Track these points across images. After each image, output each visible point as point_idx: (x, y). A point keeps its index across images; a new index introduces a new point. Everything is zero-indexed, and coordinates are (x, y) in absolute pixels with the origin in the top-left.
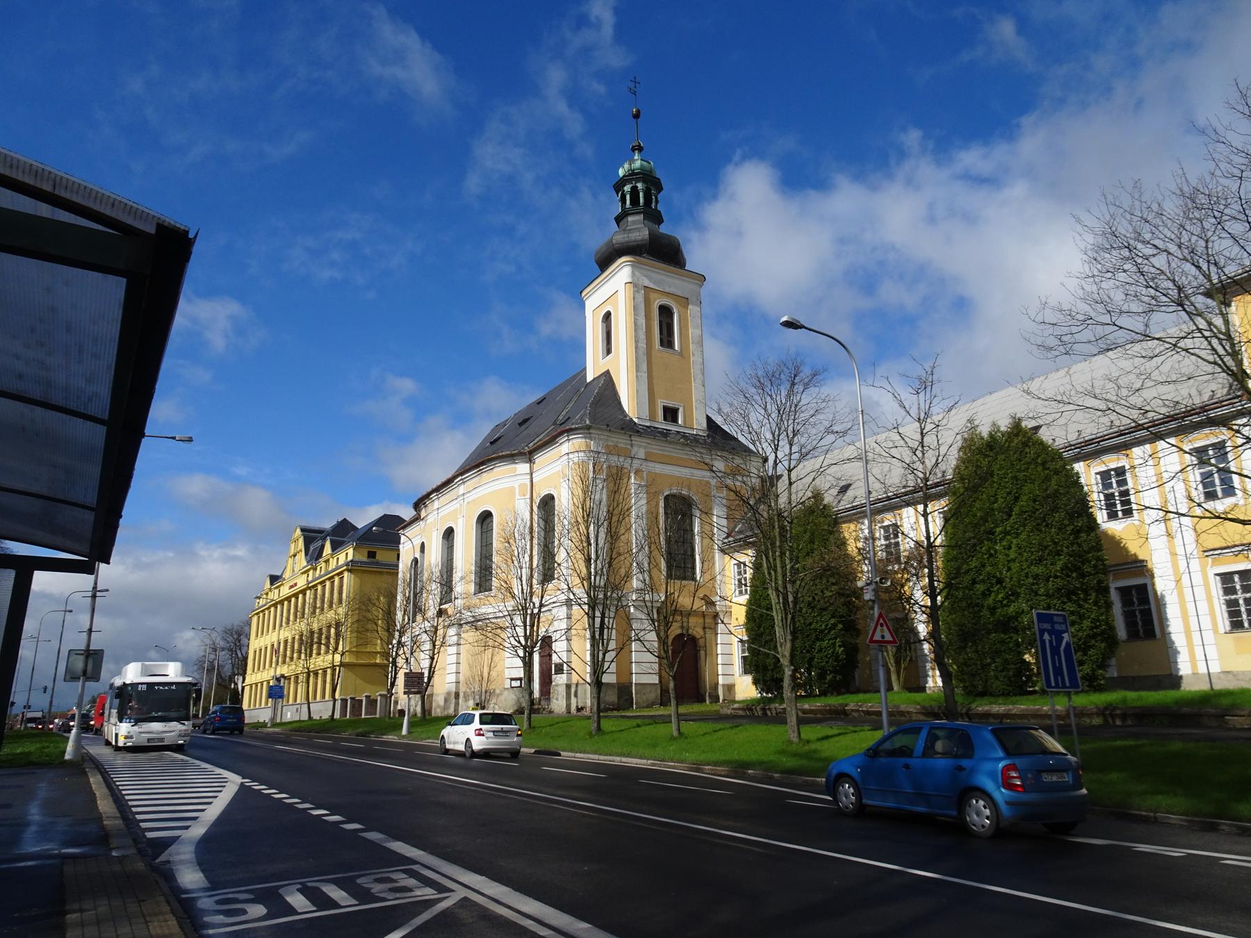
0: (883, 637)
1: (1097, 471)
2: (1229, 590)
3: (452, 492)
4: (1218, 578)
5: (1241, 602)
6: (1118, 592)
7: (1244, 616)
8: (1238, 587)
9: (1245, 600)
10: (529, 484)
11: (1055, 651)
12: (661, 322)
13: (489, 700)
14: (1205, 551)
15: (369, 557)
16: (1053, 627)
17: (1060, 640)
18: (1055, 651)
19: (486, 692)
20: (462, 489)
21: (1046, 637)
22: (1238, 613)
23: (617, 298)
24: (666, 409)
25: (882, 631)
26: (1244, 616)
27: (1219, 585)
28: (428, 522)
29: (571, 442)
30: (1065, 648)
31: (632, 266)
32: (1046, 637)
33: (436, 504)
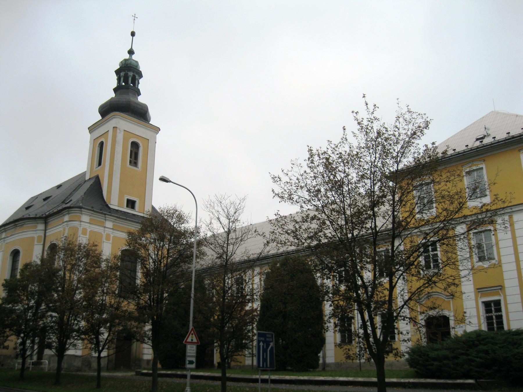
0: (192, 340)
5: (494, 317)
6: (483, 304)
7: (495, 325)
8: (493, 309)
10: (43, 236)
11: (265, 351)
12: (131, 152)
14: (478, 289)
16: (265, 339)
17: (268, 346)
18: (265, 351)
21: (261, 344)
22: (492, 324)
23: (108, 135)
24: (128, 201)
25: (192, 337)
26: (495, 325)
30: (270, 349)
32: (261, 344)
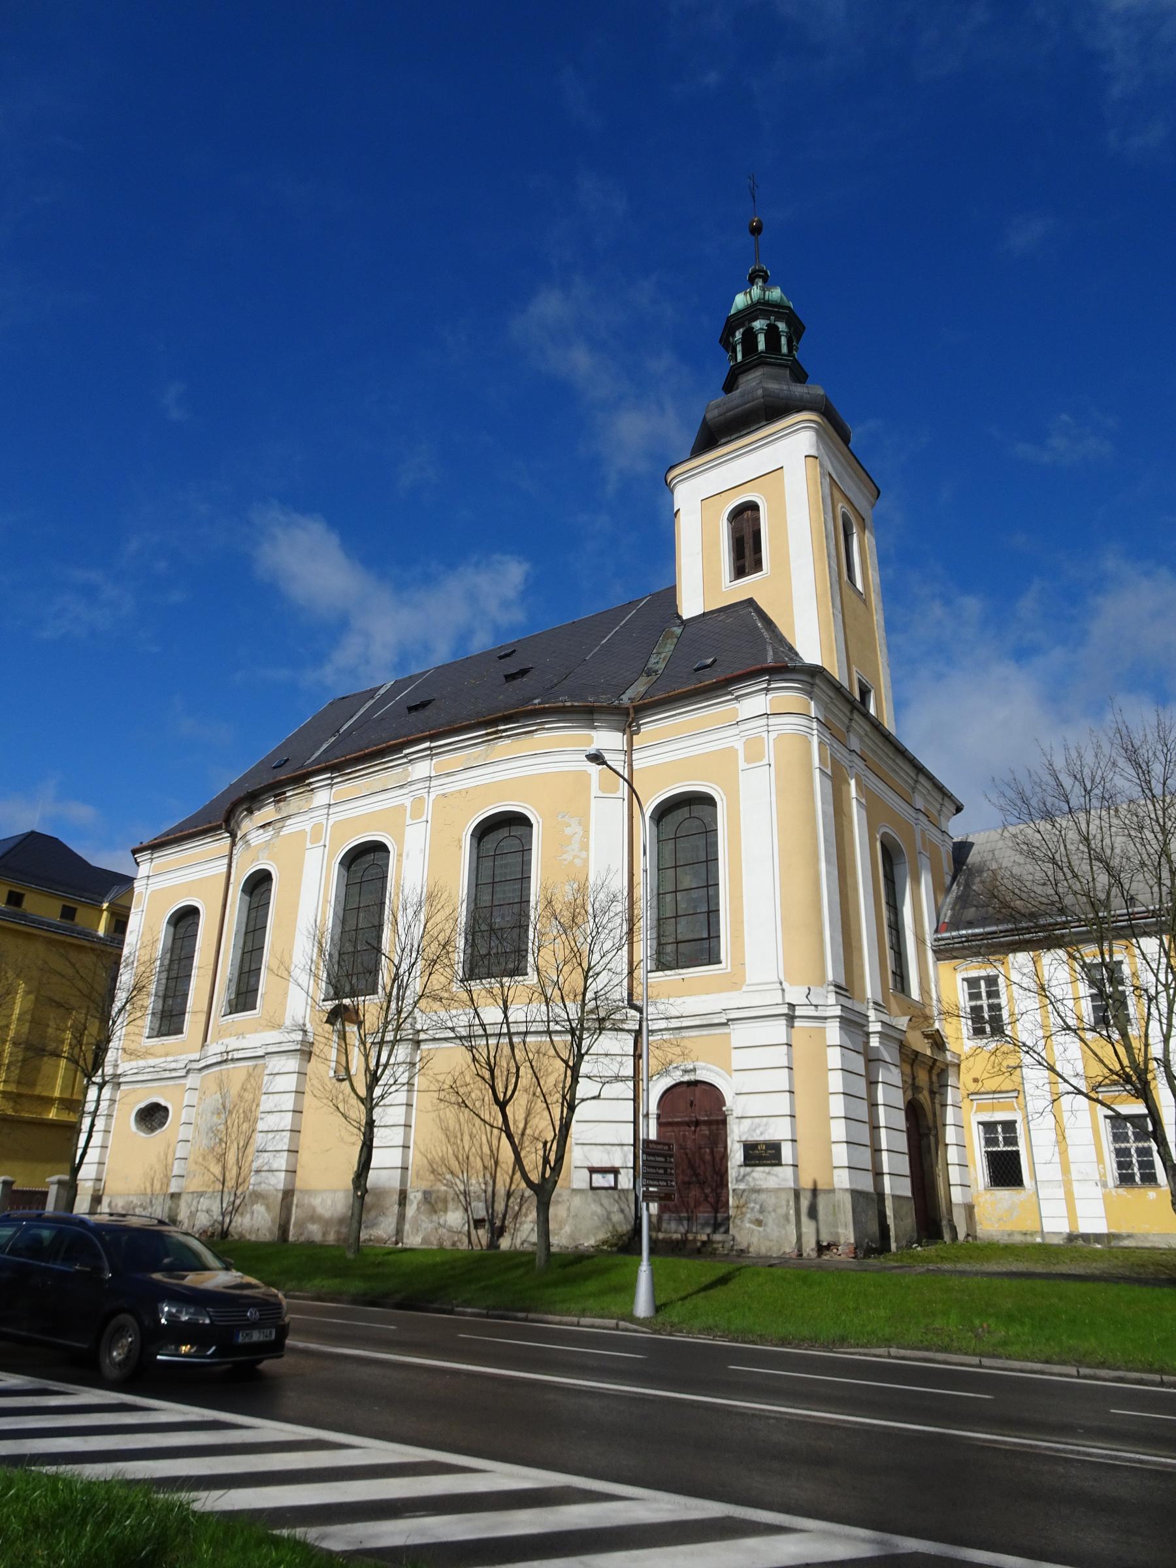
1: (966, 976)
2: (1118, 1137)
3: (377, 776)
4: (1108, 1121)
7: (1136, 1170)
8: (1001, 1139)
9: (1137, 1149)
13: (516, 1216)
15: (9, 902)
19: (509, 1195)
20: (422, 769)
26: (1136, 1170)
27: (982, 1134)
28: (284, 832)
29: (770, 697)
31: (817, 431)
33: (322, 797)
